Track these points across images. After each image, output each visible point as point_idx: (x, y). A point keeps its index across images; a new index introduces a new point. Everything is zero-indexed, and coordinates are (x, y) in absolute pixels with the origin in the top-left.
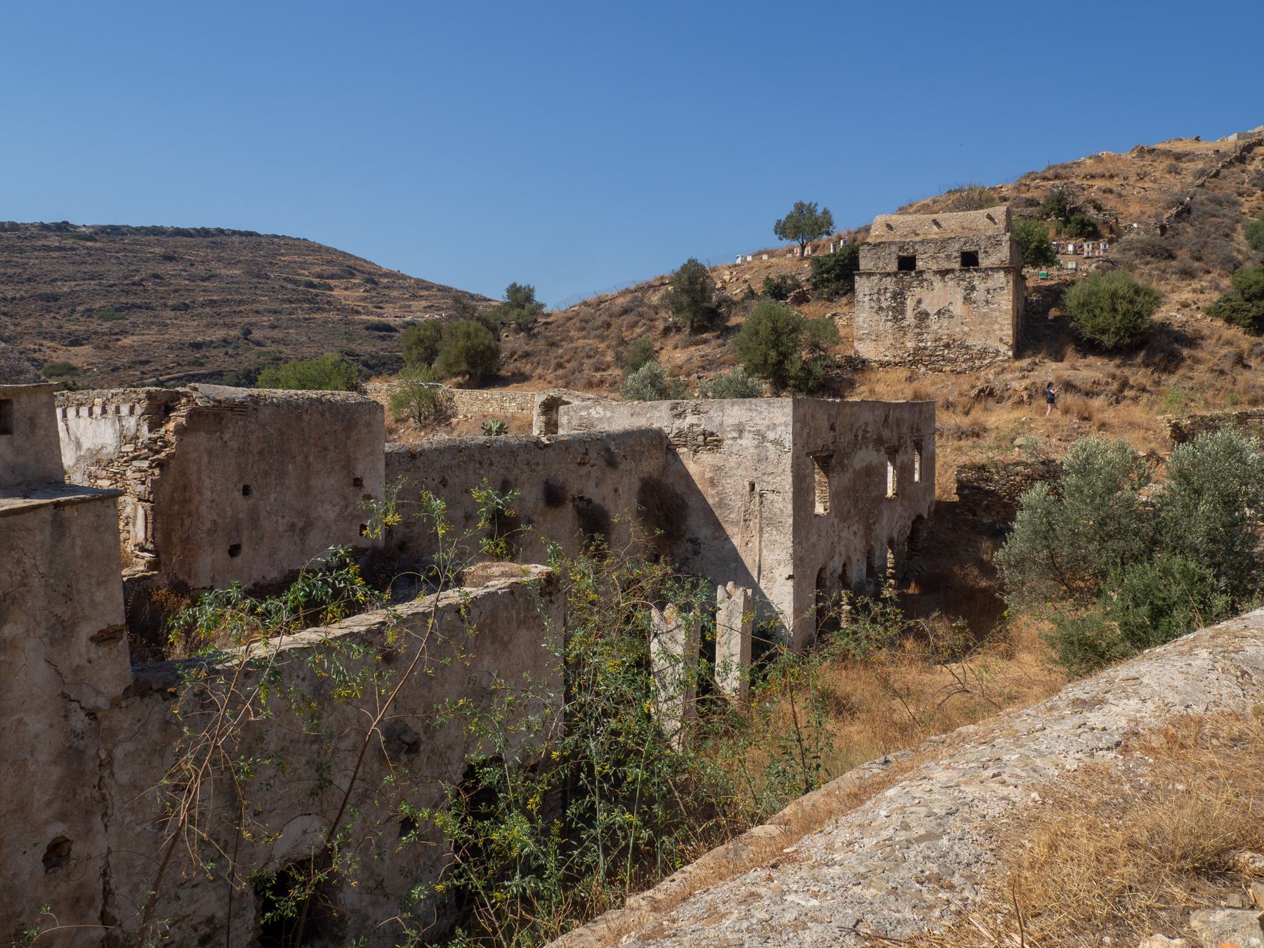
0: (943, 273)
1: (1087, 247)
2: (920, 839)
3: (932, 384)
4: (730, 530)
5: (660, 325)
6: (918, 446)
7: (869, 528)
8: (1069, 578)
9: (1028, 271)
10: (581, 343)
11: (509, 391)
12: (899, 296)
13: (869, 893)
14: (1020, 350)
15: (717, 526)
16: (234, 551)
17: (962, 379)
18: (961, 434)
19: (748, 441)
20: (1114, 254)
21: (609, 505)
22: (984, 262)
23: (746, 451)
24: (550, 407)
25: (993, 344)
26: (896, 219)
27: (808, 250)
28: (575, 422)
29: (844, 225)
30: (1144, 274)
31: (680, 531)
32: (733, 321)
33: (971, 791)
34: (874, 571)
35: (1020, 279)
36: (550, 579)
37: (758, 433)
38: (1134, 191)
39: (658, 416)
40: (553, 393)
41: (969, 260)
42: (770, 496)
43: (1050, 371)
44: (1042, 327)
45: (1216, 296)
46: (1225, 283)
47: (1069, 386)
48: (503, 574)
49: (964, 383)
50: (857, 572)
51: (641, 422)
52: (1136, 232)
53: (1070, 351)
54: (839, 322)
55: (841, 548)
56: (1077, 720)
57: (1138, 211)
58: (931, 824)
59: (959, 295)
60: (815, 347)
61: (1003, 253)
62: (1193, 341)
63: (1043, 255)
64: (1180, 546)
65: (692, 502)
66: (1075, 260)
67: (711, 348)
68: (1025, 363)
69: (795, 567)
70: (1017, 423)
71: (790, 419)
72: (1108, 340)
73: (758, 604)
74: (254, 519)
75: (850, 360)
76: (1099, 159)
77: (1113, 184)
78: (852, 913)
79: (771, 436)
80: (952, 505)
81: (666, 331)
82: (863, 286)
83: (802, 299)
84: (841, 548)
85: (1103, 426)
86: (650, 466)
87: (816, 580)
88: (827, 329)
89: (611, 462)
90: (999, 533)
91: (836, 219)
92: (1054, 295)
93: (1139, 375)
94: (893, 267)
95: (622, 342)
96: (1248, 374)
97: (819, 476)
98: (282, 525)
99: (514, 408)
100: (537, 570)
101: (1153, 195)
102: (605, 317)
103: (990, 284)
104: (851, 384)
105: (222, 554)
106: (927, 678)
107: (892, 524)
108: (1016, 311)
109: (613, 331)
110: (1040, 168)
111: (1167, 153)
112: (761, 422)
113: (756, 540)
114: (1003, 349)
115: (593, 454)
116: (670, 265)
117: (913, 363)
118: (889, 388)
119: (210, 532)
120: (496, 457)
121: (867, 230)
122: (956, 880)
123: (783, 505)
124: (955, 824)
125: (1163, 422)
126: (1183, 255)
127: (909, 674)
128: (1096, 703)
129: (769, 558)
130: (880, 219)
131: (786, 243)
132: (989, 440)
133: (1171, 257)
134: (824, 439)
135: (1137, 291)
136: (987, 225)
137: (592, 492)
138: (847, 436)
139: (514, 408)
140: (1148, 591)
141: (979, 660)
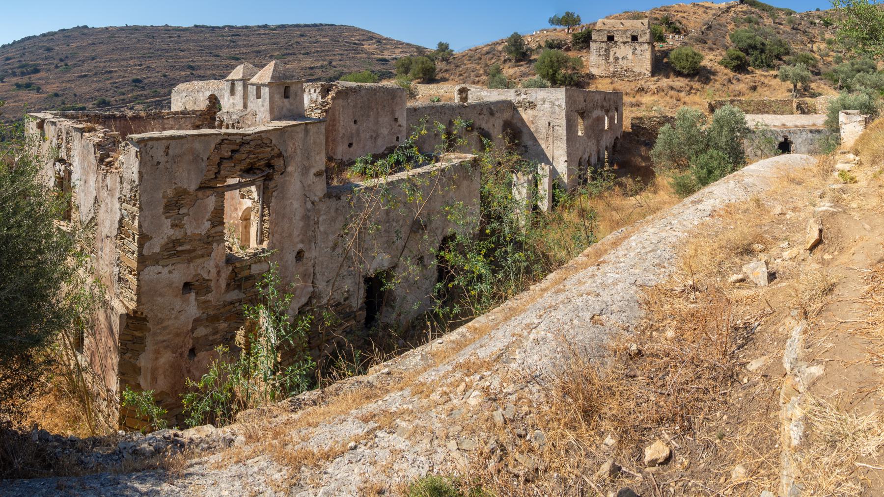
0: (625, 43)
1: (677, 37)
2: (650, 252)
3: (622, 86)
4: (540, 142)
5: (503, 59)
6: (617, 109)
7: (598, 142)
8: (678, 161)
9: (655, 43)
10: (469, 66)
11: (441, 85)
12: (607, 50)
13: (637, 271)
14: (653, 74)
15: (535, 140)
16: (350, 145)
17: (632, 84)
18: (632, 105)
19: (547, 105)
20: (686, 40)
21: (491, 131)
22: (640, 40)
23: (546, 111)
24: (463, 92)
25: (643, 71)
26: (606, 21)
27: (570, 31)
28: (475, 97)
29: (585, 21)
30: (697, 48)
31: (520, 141)
32: (533, 57)
33: (664, 234)
34: (601, 161)
35: (653, 47)
36: (475, 160)
37: (551, 102)
38: (692, 18)
39: (509, 95)
40: (463, 86)
41: (634, 38)
42: (556, 128)
43: (665, 82)
44: (661, 65)
45: (721, 58)
46: (724, 53)
47: (672, 88)
48: (456, 158)
49: (633, 85)
50: (594, 160)
51: (502, 98)
52: (694, 33)
53: (672, 75)
54: (584, 59)
55: (588, 150)
56: (694, 208)
57: (695, 23)
58: (653, 246)
59: (631, 51)
60: (574, 69)
61: (647, 37)
62: (714, 73)
63: (661, 39)
64: (717, 147)
65: (524, 130)
66: (672, 41)
67: (524, 68)
68: (655, 78)
69: (568, 157)
70: (653, 101)
71: (564, 97)
72: (685, 72)
73: (554, 173)
74: (358, 133)
75: (587, 74)
76: (680, 6)
77: (685, 15)
78: (632, 279)
79: (557, 103)
80: (629, 133)
81: (505, 61)
82: (593, 46)
83: (568, 49)
84: (588, 150)
85: (685, 103)
86: (507, 115)
87: (578, 162)
88: (579, 61)
89: (492, 114)
90: (650, 145)
91: (582, 19)
92: (666, 54)
93: (696, 85)
94: (605, 39)
95: (487, 65)
96: (733, 86)
97: (580, 120)
98: (368, 136)
99: (447, 92)
100: (469, 157)
101: (698, 20)
102: (479, 55)
103: (642, 48)
104: (588, 84)
105: (346, 146)
106: (624, 202)
107: (607, 140)
108: (652, 59)
109: (483, 61)
110: (659, 7)
111: (703, 6)
112: (553, 98)
113: (551, 146)
114: (647, 73)
115: (485, 110)
116: (506, 35)
117: (613, 77)
118: (603, 86)
119: (342, 138)
120: (437, 110)
121: (595, 24)
122: (666, 264)
123: (562, 131)
124: (661, 245)
125: (705, 102)
126: (709, 42)
127: (617, 201)
128: (700, 201)
129: (557, 153)
130: (600, 21)
131: (554, 27)
132: (643, 107)
133: (706, 43)
134: (581, 105)
135: (695, 54)
136: (641, 26)
137: (484, 126)
138: (589, 106)
139: (447, 92)
140: (707, 164)
141: (644, 194)
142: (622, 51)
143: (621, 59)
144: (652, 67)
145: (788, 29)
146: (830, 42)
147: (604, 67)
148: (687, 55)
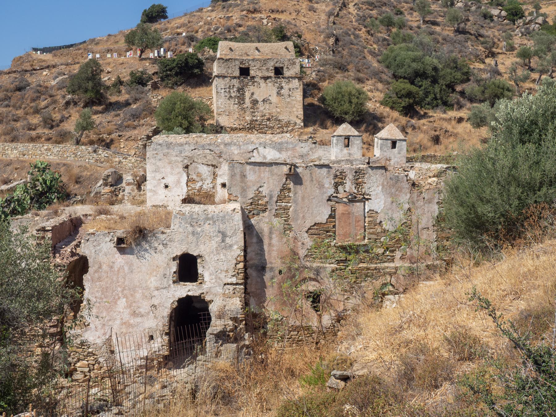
0: (266, 78)
12: (241, 90)
22: (287, 73)
25: (293, 119)
41: (278, 72)
53: (329, 123)
59: (275, 91)
68: (310, 129)
94: (237, 73)
142: (264, 90)
143: (260, 103)
144: (305, 115)
145: (449, 32)
146: (525, 55)
147: (236, 116)
148: (350, 94)
